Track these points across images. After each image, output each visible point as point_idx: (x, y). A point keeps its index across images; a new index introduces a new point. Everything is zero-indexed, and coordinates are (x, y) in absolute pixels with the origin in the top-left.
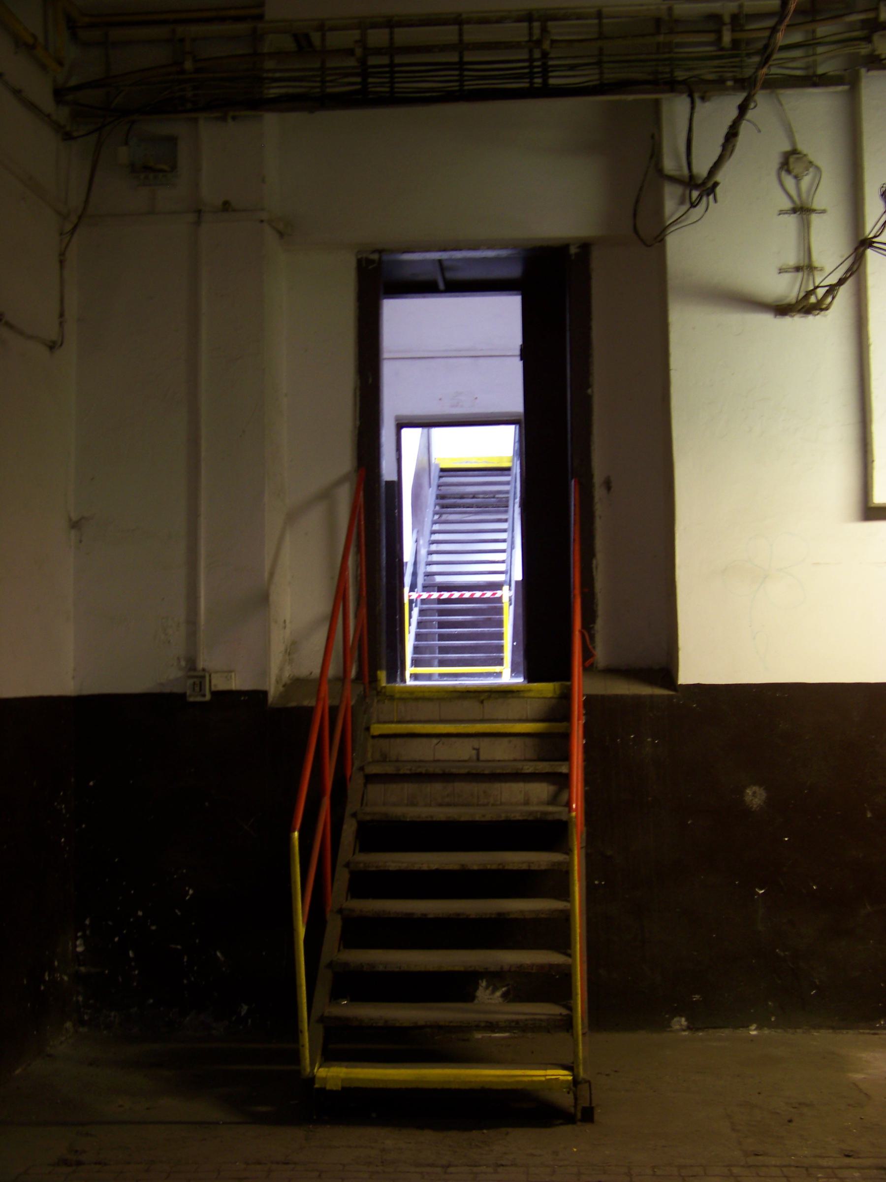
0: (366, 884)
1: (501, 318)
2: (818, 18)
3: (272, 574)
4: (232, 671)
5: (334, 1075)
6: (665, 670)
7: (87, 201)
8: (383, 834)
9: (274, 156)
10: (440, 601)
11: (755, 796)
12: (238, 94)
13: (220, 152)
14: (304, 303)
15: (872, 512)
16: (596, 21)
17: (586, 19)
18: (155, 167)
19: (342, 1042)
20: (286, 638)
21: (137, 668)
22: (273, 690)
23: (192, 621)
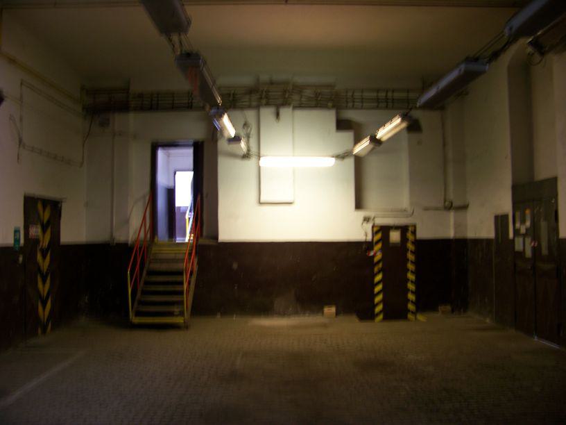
0: (142, 303)
1: (190, 151)
2: (129, 213)
3: (130, 214)
4: (120, 237)
5: (136, 320)
6: (216, 237)
7: (89, 131)
8: (152, 273)
9: (133, 120)
10: (171, 314)
11: (235, 266)
12: (124, 107)
13: (118, 120)
14: (137, 156)
15: (260, 203)
18: (104, 124)
19: (138, 314)
20: (132, 228)
21: (99, 236)
22: (130, 243)
23: (112, 228)
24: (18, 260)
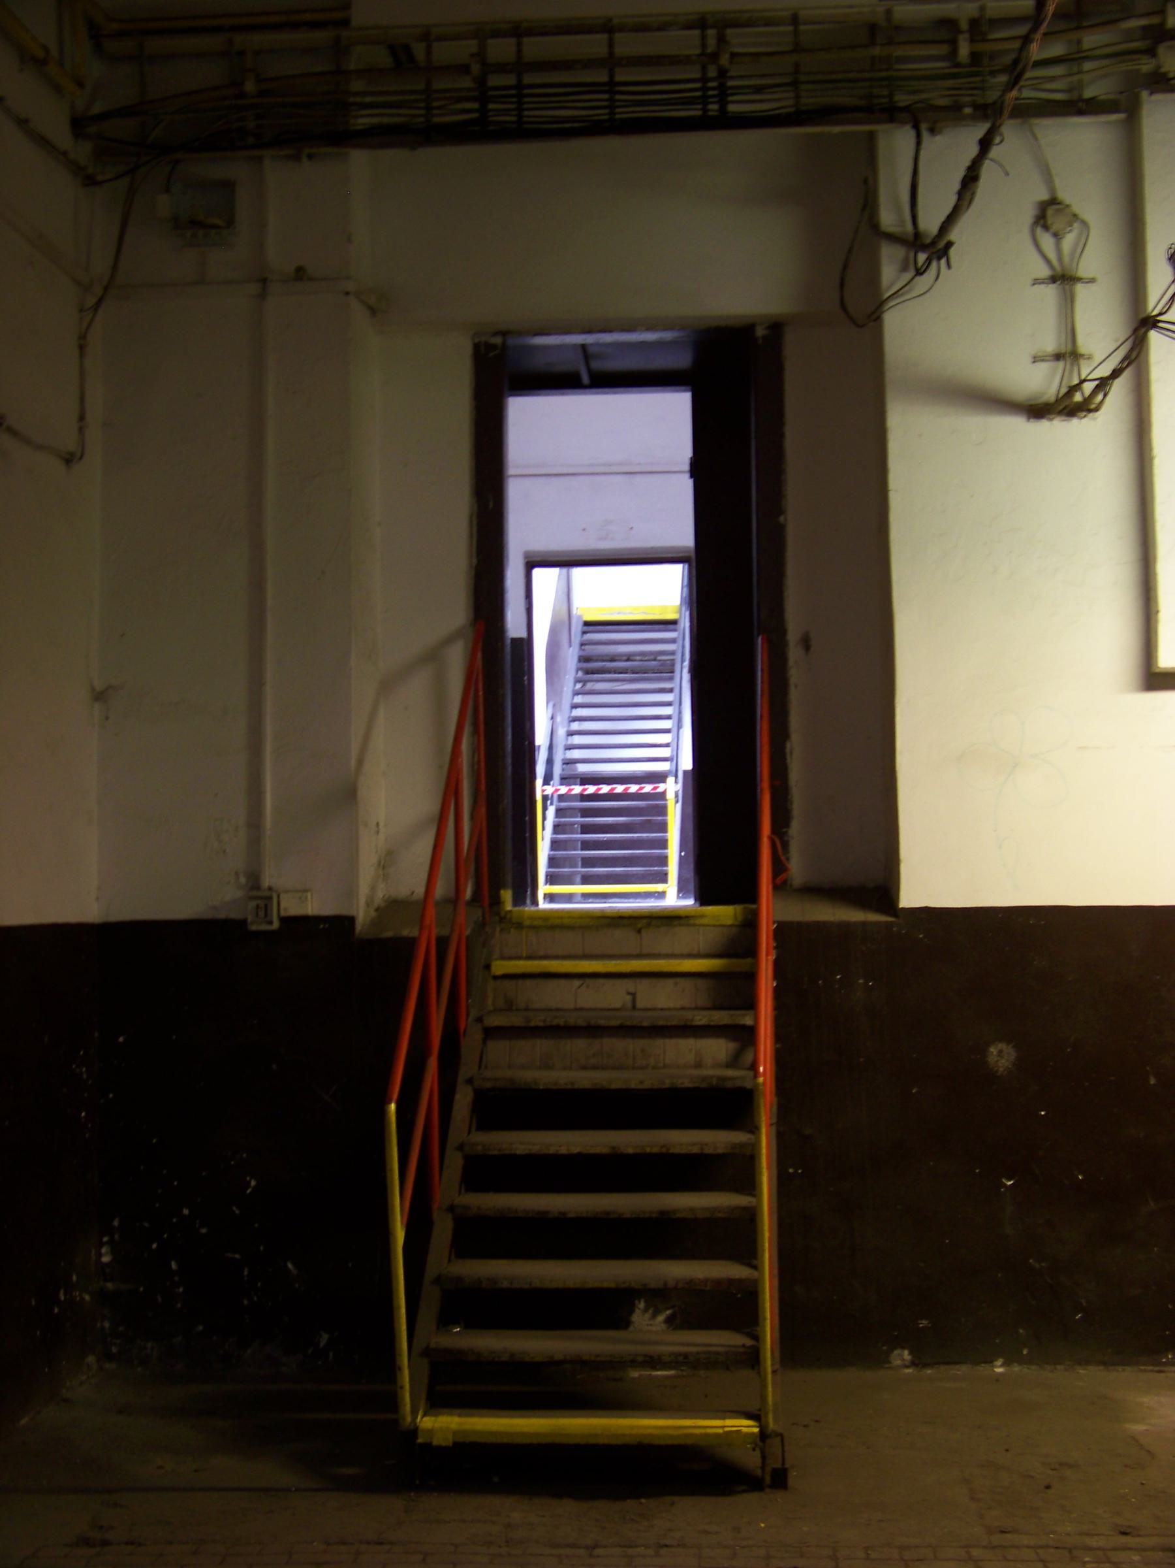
1: (664, 422)
2: (1085, 24)
3: (360, 762)
4: (307, 890)
5: (442, 1426)
6: (882, 889)
7: (115, 267)
8: (508, 1106)
9: (363, 207)
11: (1001, 1056)
12: (316, 125)
13: (292, 201)
14: (404, 402)
15: (1156, 679)
18: (206, 222)
19: (454, 1382)
20: (379, 846)
21: (182, 887)
22: (362, 915)
23: (255, 824)
24: (1000, 1374)
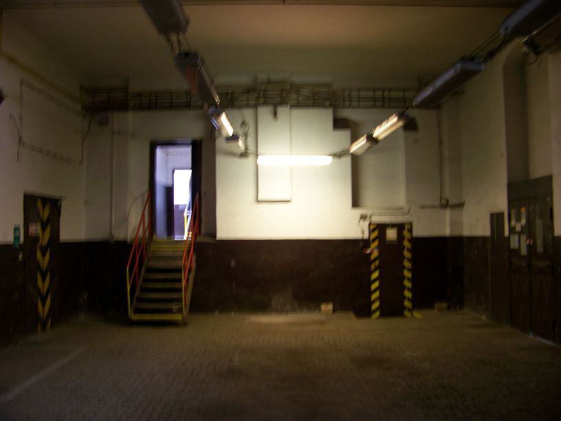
0: (141, 300)
1: (188, 150)
2: (128, 211)
3: (129, 212)
4: (119, 235)
5: (135, 317)
6: (214, 235)
7: (89, 129)
8: (150, 270)
9: (132, 119)
11: (233, 263)
12: (123, 106)
13: (117, 119)
14: (135, 155)
15: (258, 201)
16: (357, 93)
17: (436, 76)
18: (103, 123)
19: (137, 311)
20: (131, 226)
21: (99, 234)
22: (128, 240)
23: (111, 226)
24: (18, 257)
